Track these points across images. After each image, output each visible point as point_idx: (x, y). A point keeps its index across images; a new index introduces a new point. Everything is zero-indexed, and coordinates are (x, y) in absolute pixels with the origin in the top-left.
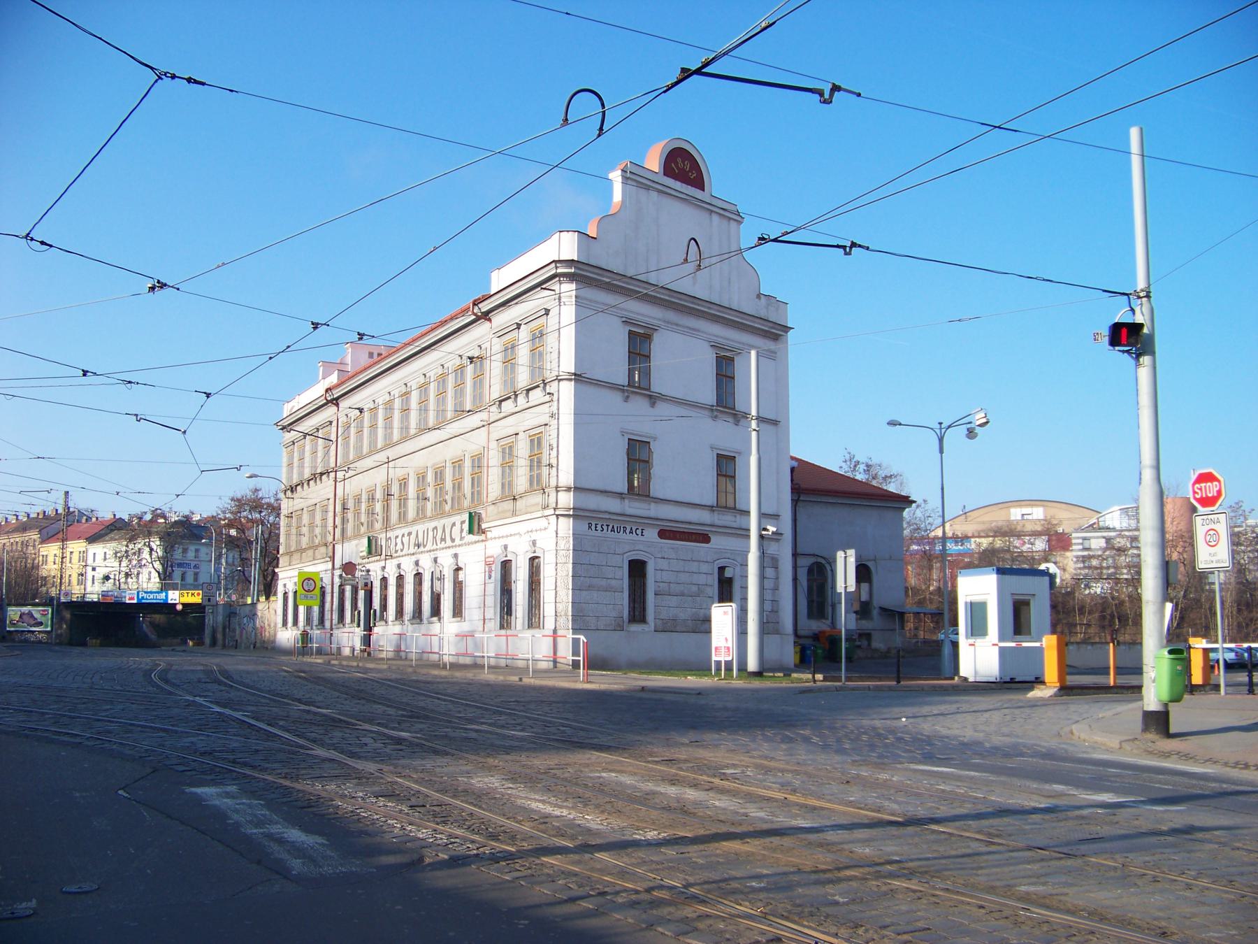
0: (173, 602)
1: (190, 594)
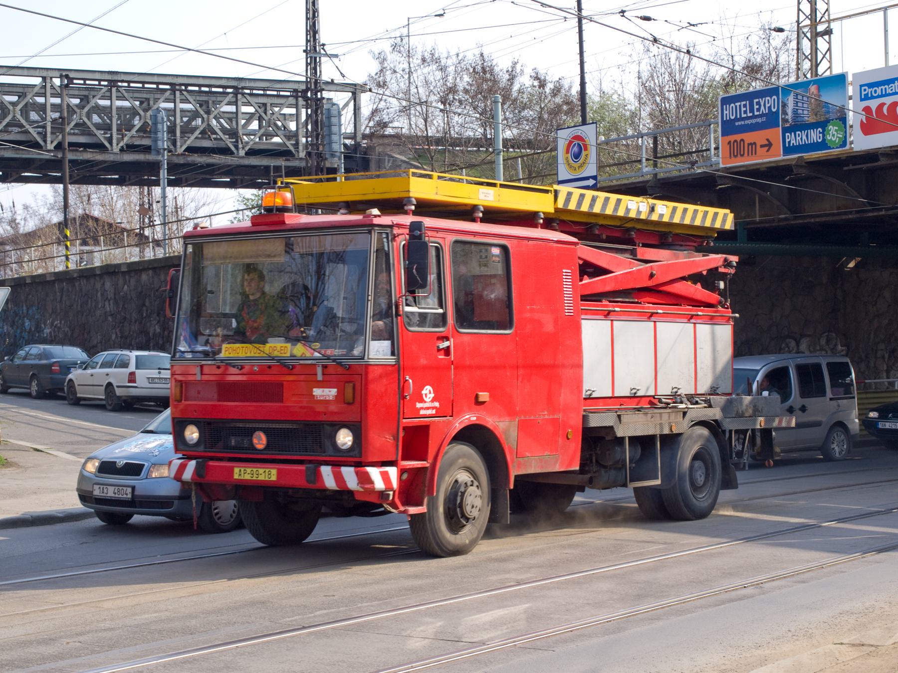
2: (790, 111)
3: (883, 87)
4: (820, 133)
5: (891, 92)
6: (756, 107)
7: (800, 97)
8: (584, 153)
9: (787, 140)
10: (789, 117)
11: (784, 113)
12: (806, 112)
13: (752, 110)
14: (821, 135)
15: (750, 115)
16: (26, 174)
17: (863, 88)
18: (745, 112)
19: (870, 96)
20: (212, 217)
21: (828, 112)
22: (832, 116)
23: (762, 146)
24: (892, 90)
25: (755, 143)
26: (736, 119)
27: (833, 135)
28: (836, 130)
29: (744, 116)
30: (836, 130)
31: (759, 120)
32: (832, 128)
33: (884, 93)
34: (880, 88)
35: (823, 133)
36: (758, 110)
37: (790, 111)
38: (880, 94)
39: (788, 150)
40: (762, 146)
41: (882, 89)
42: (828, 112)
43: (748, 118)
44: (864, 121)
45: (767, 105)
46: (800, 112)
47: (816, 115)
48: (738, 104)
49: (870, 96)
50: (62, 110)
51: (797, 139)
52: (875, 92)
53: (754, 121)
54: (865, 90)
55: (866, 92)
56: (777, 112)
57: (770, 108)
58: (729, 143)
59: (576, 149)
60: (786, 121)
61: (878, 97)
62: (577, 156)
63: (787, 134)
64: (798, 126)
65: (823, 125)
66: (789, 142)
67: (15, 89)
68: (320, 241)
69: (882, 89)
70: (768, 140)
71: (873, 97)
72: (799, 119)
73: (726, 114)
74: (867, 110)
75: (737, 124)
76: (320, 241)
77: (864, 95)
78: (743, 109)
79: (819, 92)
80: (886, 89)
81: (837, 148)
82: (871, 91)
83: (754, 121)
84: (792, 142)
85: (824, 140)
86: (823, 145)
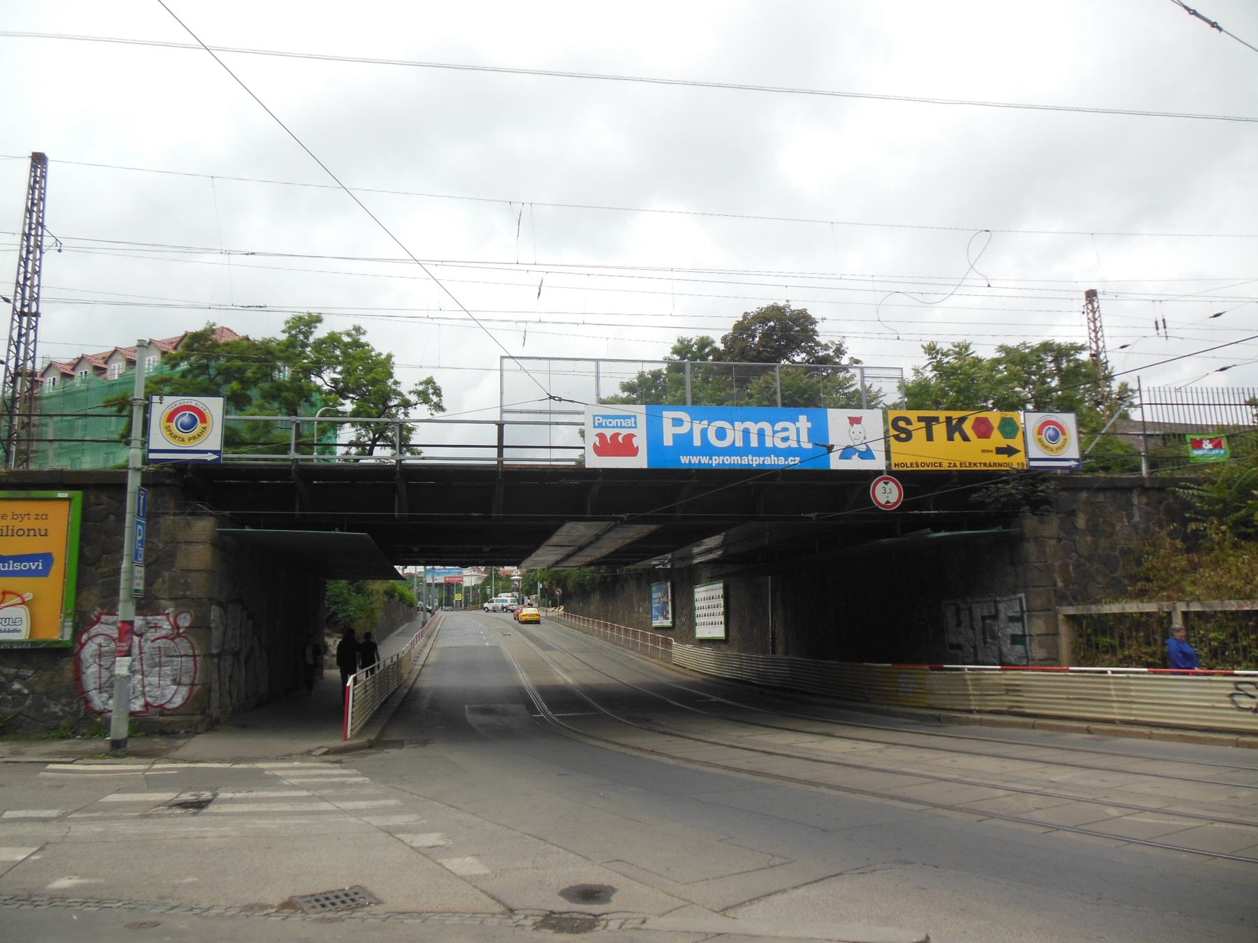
0: (855, 464)
1: (940, 430)
5: (782, 445)
16: (473, 514)
17: (596, 418)
19: (697, 442)
20: (601, 363)
41: (746, 432)
52: (721, 434)
54: (599, 420)
55: (683, 430)
61: (613, 427)
68: (598, 367)
71: (606, 427)
73: (1106, 672)
74: (601, 436)
76: (598, 367)
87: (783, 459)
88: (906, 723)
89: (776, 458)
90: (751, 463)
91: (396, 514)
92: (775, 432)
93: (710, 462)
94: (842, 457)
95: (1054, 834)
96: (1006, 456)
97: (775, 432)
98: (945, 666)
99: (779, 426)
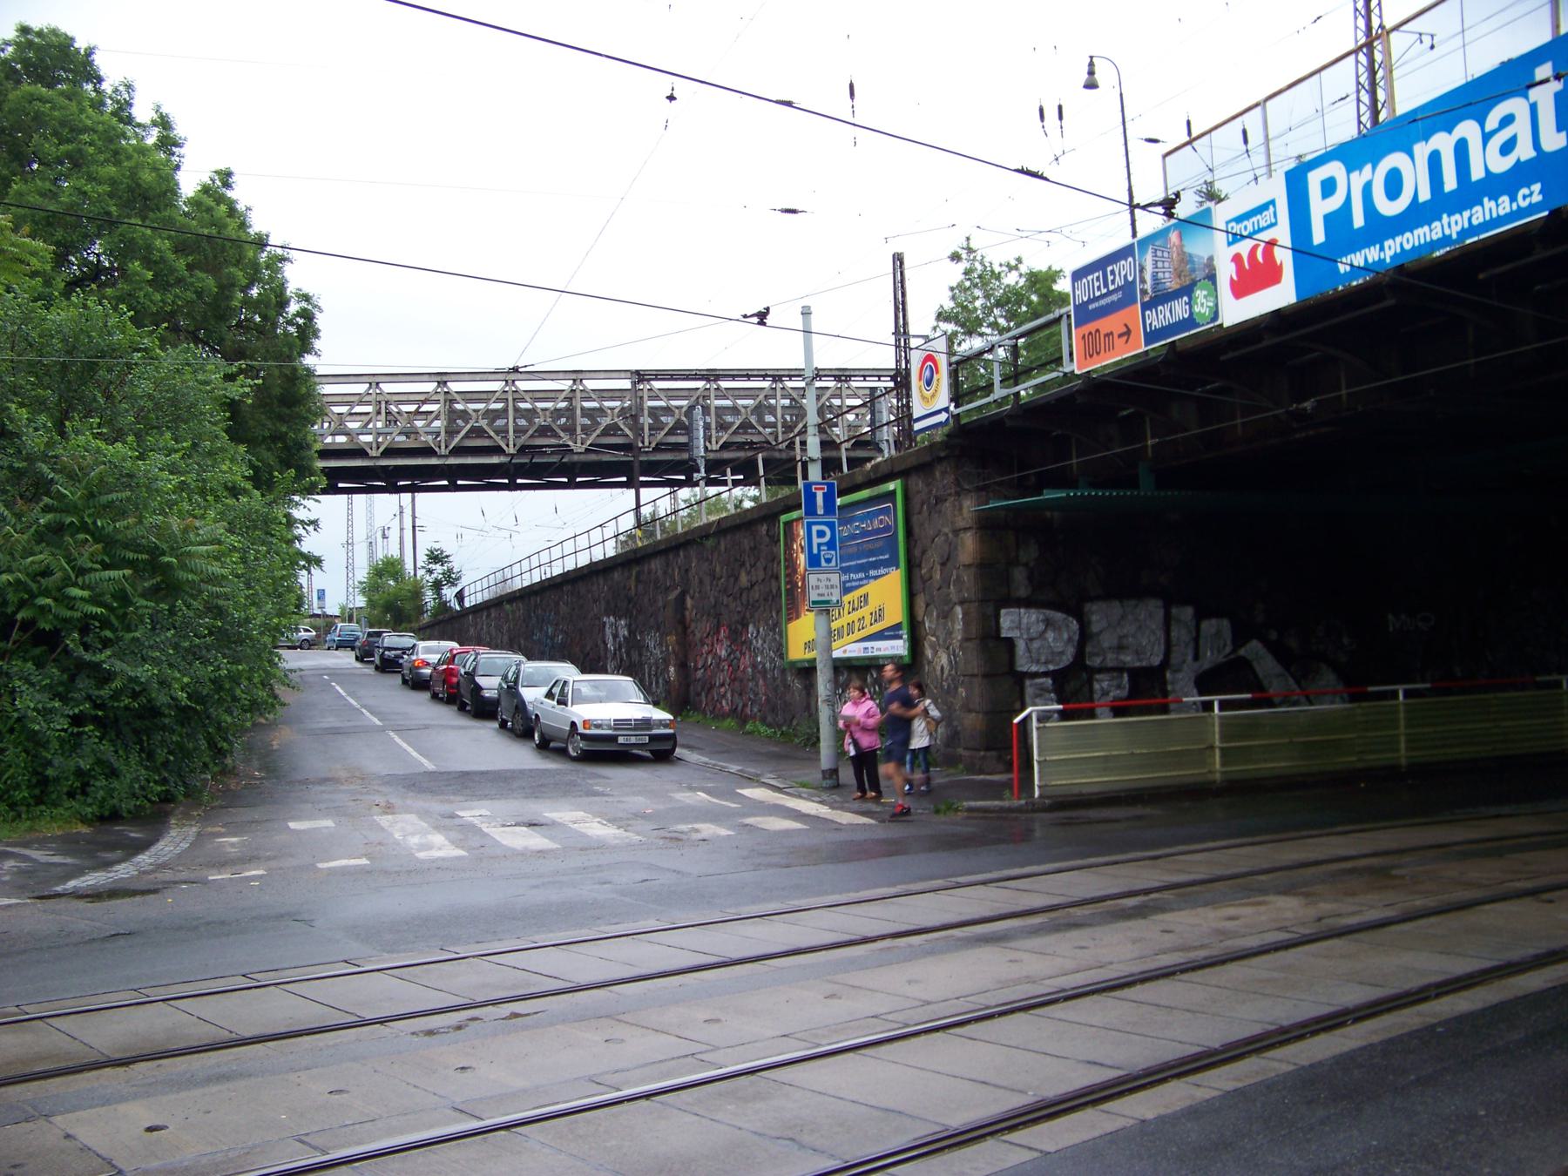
2: (1148, 277)
3: (1443, 143)
4: (1186, 304)
5: (1265, 225)
6: (1110, 278)
7: (1159, 253)
8: (935, 376)
9: (1148, 322)
10: (1148, 286)
11: (1143, 281)
12: (1167, 275)
13: (1106, 285)
14: (1187, 307)
15: (1104, 291)
18: (1099, 288)
19: (1358, 221)
21: (1193, 270)
22: (1199, 275)
23: (1120, 336)
24: (1507, 148)
25: (1112, 333)
26: (1090, 301)
27: (1202, 304)
28: (1205, 297)
29: (1097, 294)
30: (1205, 297)
31: (1114, 297)
32: (1200, 294)
33: (1450, 183)
34: (1422, 150)
35: (1189, 303)
36: (1113, 282)
37: (1148, 277)
38: (1425, 195)
39: (1151, 336)
40: (1120, 336)
41: (1435, 160)
42: (1193, 270)
43: (1103, 296)
44: (1235, 278)
45: (1123, 273)
46: (1160, 275)
47: (1179, 277)
48: (1090, 278)
49: (1358, 221)
50: (449, 412)
51: (1160, 317)
52: (1394, 185)
53: (1108, 300)
55: (1335, 202)
56: (1134, 281)
57: (1125, 276)
58: (1084, 337)
59: (927, 373)
60: (1144, 292)
62: (929, 383)
63: (1148, 312)
64: (1161, 298)
65: (1187, 291)
66: (1151, 324)
67: (412, 397)
69: (1435, 160)
70: (1126, 325)
72: (1160, 287)
75: (1091, 307)
77: (1328, 219)
78: (1096, 284)
79: (1181, 240)
80: (1461, 148)
81: (1208, 323)
82: (1367, 189)
83: (1108, 300)
84: (1154, 324)
85: (1191, 314)
86: (1190, 322)
87: (1505, 199)
88: (1497, 816)
89: (1493, 204)
90: (1447, 232)
91: (1344, 392)
92: (1486, 137)
93: (1382, 256)
94: (1241, 288)
95: (781, 786)
96: (1522, 159)
97: (1486, 137)
98: (1371, 689)
99: (1492, 121)
